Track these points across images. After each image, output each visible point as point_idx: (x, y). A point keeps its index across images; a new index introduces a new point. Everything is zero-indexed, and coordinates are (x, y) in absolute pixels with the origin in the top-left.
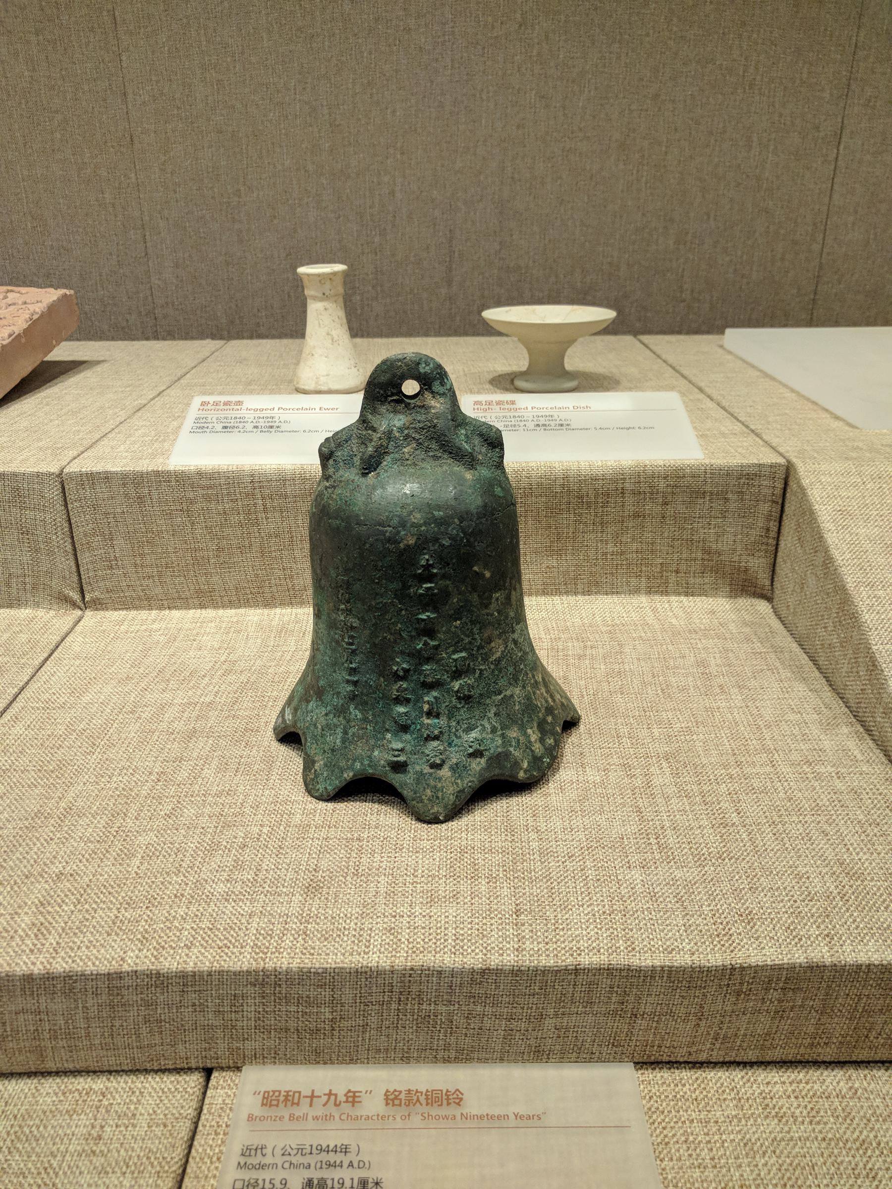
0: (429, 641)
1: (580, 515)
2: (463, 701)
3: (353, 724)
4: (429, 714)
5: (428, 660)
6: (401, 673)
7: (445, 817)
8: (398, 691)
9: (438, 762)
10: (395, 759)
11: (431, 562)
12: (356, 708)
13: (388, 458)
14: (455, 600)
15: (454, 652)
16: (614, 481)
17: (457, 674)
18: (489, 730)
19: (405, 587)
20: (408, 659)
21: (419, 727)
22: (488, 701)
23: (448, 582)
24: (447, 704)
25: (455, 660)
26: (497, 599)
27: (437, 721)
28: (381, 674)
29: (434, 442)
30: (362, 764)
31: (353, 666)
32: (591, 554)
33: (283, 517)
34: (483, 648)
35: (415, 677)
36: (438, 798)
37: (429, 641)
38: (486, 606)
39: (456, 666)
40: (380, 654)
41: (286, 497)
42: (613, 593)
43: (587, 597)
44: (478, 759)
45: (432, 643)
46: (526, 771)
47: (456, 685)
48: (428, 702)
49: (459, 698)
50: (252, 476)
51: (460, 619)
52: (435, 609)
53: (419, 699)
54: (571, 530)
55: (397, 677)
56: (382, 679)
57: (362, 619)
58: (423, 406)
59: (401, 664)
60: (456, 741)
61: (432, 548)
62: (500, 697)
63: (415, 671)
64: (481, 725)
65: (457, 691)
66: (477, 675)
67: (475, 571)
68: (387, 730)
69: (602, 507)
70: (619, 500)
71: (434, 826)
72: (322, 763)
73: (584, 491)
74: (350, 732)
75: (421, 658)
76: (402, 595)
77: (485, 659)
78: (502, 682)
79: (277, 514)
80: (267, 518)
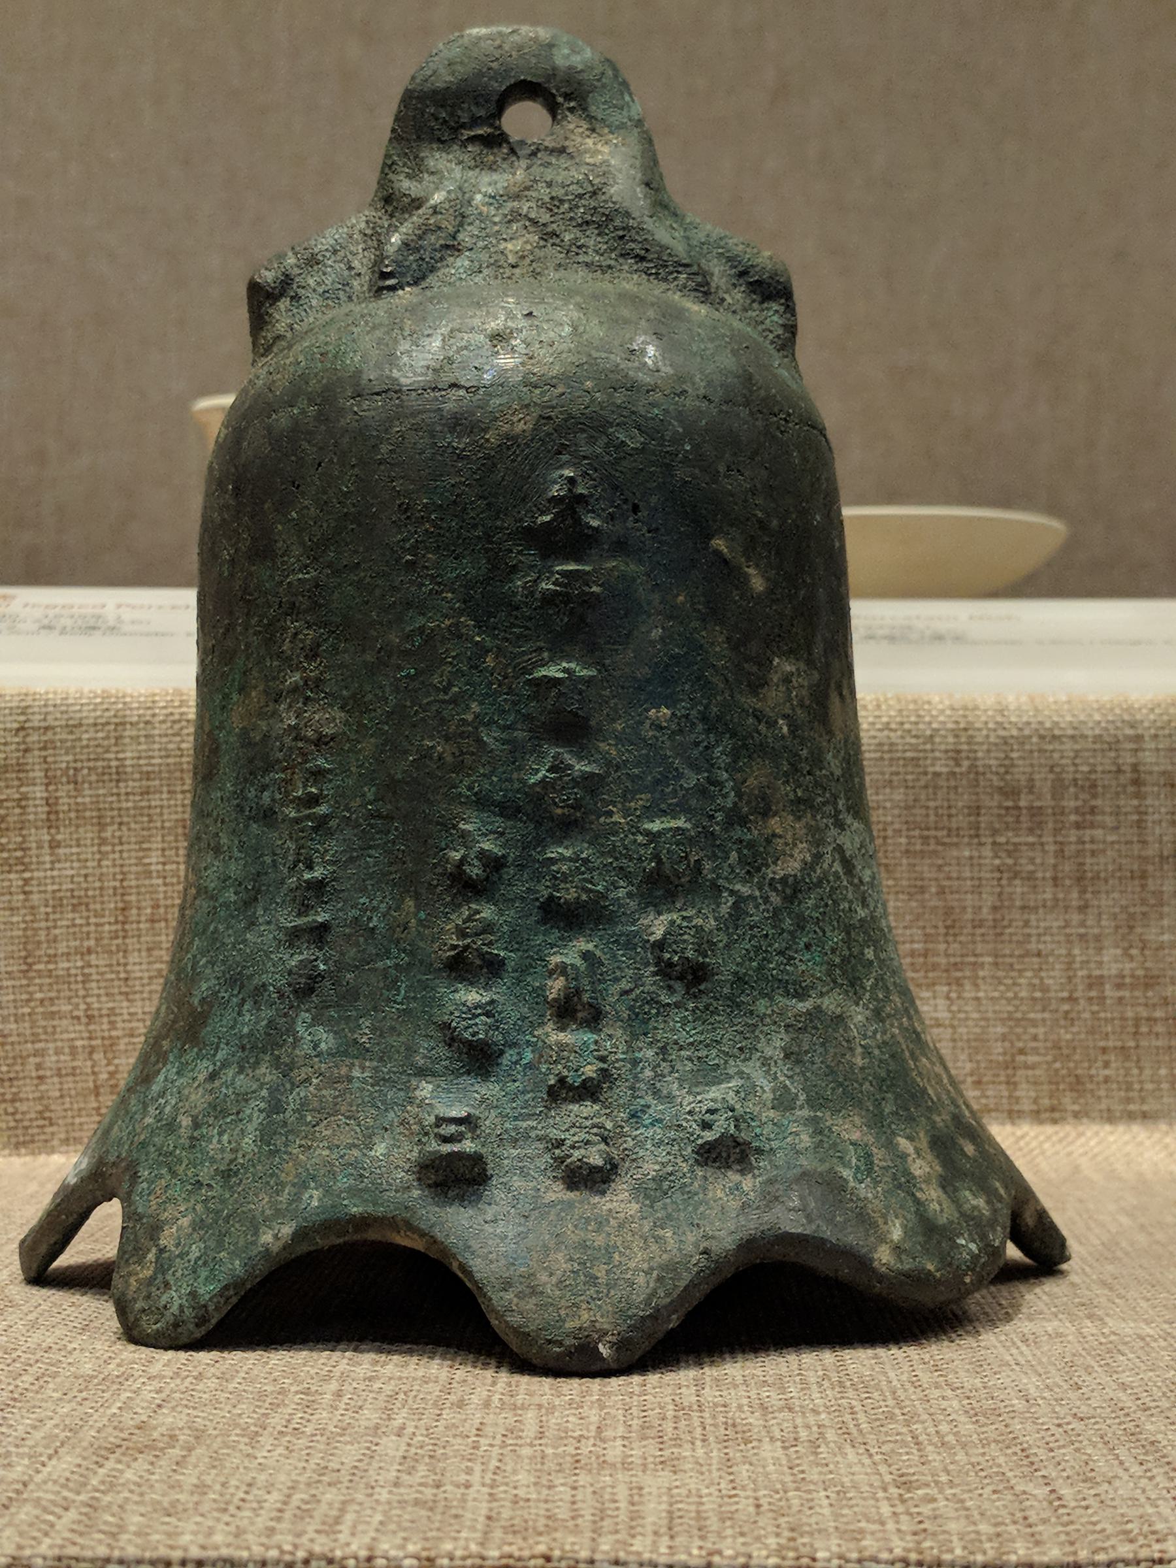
0: (569, 759)
1: (1014, 850)
2: (678, 985)
3: (304, 1072)
4: (566, 1011)
5: (567, 828)
6: (475, 871)
7: (621, 1345)
8: (462, 934)
9: (596, 1160)
10: (447, 1148)
11: (580, 490)
12: (316, 1021)
13: (462, 262)
14: (656, 633)
15: (651, 812)
16: (1109, 743)
17: (661, 887)
18: (769, 1096)
19: (502, 570)
20: (499, 823)
21: (529, 1056)
22: (762, 1006)
23: (633, 568)
24: (624, 985)
25: (653, 836)
26: (787, 680)
27: (589, 1037)
28: (408, 884)
29: (592, 231)
30: (328, 1191)
31: (318, 873)
32: (1054, 978)
33: (103, 841)
34: (743, 821)
35: (519, 889)
36: (593, 1280)
37: (569, 759)
38: (757, 686)
39: (656, 857)
40: (406, 813)
41: (120, 775)
42: (1131, 1117)
43: (1049, 1129)
44: (733, 1177)
45: (581, 767)
46: (897, 1249)
47: (658, 926)
48: (562, 969)
49: (665, 970)
50: (24, 711)
51: (671, 701)
52: (591, 652)
53: (533, 962)
54: (988, 900)
55: (467, 887)
56: (410, 903)
57: (354, 705)
58: (562, 151)
59: (480, 837)
60: (657, 1108)
61: (585, 450)
62: (803, 1006)
63: (522, 867)
64: (741, 1074)
65: (660, 945)
66: (724, 910)
67: (717, 553)
68: (422, 1073)
69: (1078, 826)
70: (1128, 804)
71: (572, 1386)
72: (185, 1222)
73: (1020, 774)
74: (292, 1100)
75: (545, 817)
76: (487, 604)
77: (753, 864)
78: (807, 965)
79: (88, 834)
80: (54, 845)
